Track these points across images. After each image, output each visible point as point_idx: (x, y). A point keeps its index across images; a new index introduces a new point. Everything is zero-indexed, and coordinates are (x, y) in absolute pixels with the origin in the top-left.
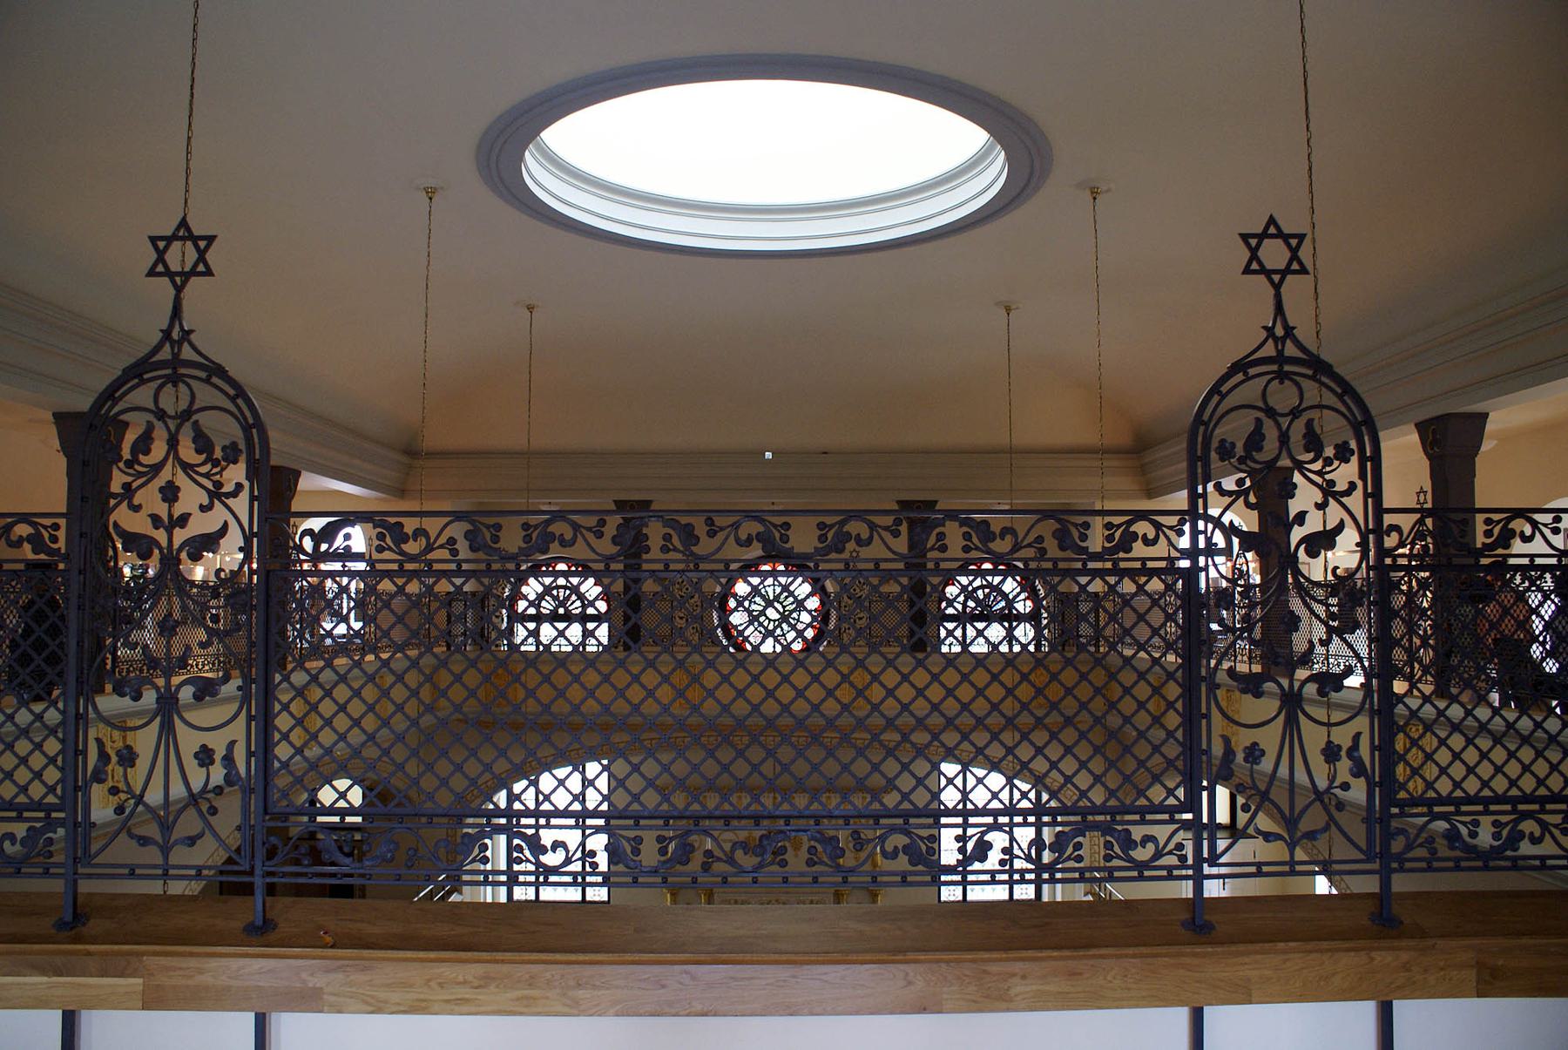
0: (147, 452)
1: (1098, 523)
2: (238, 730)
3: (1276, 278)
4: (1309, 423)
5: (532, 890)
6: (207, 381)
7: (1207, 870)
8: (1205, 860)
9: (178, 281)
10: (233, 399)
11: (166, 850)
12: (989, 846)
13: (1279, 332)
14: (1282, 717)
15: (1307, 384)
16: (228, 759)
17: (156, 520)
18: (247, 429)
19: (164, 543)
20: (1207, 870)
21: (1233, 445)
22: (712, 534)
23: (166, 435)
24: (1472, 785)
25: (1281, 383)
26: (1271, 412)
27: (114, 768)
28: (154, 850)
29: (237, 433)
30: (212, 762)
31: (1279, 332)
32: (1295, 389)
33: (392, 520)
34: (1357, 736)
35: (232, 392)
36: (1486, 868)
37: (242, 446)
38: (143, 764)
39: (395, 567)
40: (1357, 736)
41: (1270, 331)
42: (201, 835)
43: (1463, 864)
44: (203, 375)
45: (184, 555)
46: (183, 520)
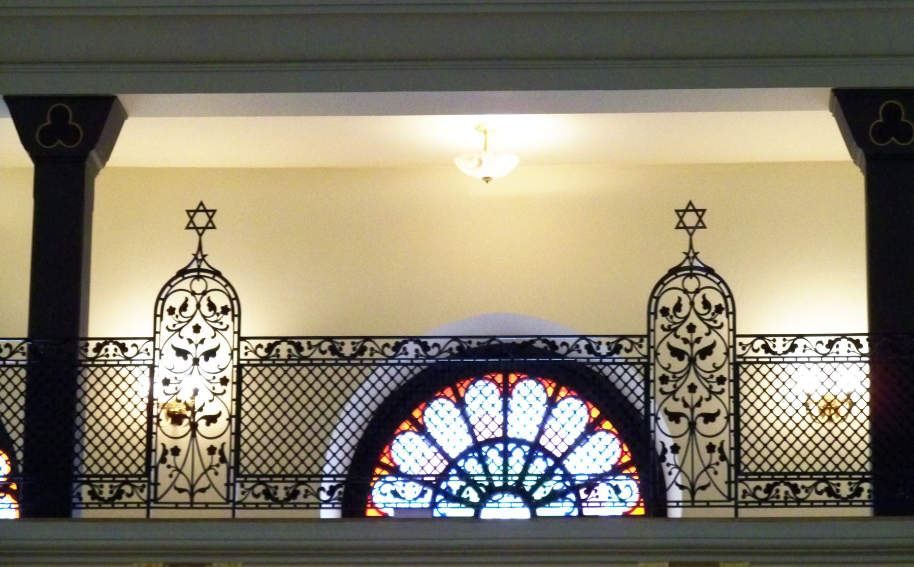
0: (680, 311)
1: (348, 342)
2: (725, 436)
4: (704, 297)
5: (732, 510)
7: (152, 504)
9: (201, 231)
10: (718, 284)
11: (192, 494)
12: (861, 490)
13: (200, 257)
15: (702, 279)
17: (686, 341)
19: (689, 352)
22: (310, 348)
26: (685, 291)
27: (170, 457)
31: (200, 257)
33: (296, 341)
34: (223, 445)
35: (224, 284)
36: (282, 508)
37: (724, 306)
38: (682, 451)
39: (384, 362)
40: (223, 445)
41: (687, 254)
42: (208, 488)
44: (211, 276)
46: (698, 340)
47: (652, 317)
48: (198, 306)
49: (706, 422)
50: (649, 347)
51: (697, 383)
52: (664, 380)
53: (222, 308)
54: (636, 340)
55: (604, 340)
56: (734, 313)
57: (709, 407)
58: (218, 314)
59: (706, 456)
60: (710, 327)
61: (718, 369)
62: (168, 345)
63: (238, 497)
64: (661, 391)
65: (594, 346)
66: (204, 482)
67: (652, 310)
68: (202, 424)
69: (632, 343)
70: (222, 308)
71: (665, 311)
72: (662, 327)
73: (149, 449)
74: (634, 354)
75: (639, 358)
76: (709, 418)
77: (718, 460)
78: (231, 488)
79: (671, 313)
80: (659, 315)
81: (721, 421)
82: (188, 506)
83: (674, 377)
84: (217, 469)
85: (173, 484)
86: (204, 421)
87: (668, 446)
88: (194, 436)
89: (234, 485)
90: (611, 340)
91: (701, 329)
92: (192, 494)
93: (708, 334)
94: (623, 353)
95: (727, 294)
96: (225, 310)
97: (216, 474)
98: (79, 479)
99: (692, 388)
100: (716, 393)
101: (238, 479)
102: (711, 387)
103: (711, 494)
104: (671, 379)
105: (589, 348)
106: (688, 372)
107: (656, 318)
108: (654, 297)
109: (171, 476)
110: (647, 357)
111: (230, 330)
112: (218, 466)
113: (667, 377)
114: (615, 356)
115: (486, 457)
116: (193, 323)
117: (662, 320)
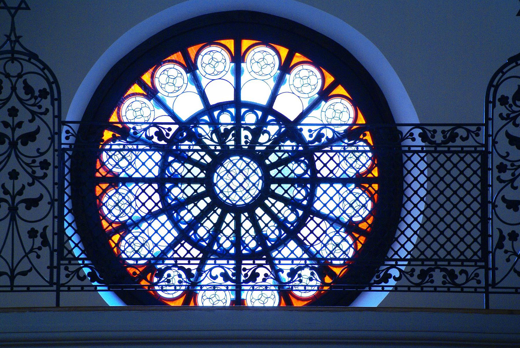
2: (48, 221)
3: (13, 11)
6: (29, 61)
7: (490, 289)
8: (490, 285)
10: (43, 70)
11: (12, 278)
13: (13, 38)
14: (9, 217)
16: (44, 235)
18: (50, 84)
20: (490, 289)
21: (507, 98)
23: (10, 86)
24: (455, 254)
25: (13, 62)
26: (8, 76)
27: (507, 244)
28: (5, 277)
29: (45, 85)
30: (36, 237)
31: (13, 38)
32: (19, 64)
34: (45, 228)
35: (42, 67)
37: (48, 90)
40: (45, 228)
42: (30, 270)
43: (412, 289)
45: (19, 141)
46: (20, 125)
47: (491, 105)
48: (14, 89)
49: (28, 208)
50: (487, 136)
51: (19, 169)
52: (502, 168)
53: (40, 91)
54: (473, 128)
55: (439, 129)
56: (59, 100)
57: (30, 193)
58: (36, 98)
59: (28, 243)
60: (33, 113)
61: (42, 154)
62: (503, 133)
63: (63, 280)
64: (499, 178)
65: (429, 135)
66: (24, 266)
67: (491, 99)
68: (22, 207)
69: (468, 131)
70: (40, 91)
71: (504, 100)
72: (501, 115)
73: (485, 234)
74: (471, 142)
75: (475, 147)
76: (32, 203)
77: (40, 245)
78: (55, 271)
79: (510, 101)
80: (498, 103)
81: (44, 206)
82: (9, 289)
83: (512, 165)
84: (39, 252)
85: (513, 268)
86: (24, 205)
87: (505, 234)
88: (13, 220)
89: (58, 268)
90: (447, 128)
91: (24, 115)
92: (12, 278)
93: (31, 121)
94: (458, 142)
95: (52, 80)
96: (43, 94)
97: (38, 257)
98: (342, 262)
99: (13, 175)
100: (38, 179)
101: (62, 262)
102: (34, 172)
103: (32, 279)
104: (509, 167)
105: (423, 136)
106: (9, 156)
107: (494, 106)
108: (493, 85)
109: (508, 260)
110: (486, 145)
111: (50, 114)
112: (40, 248)
113: (506, 166)
114: (450, 144)
115: (233, 244)
116: (9, 105)
117: (500, 109)
